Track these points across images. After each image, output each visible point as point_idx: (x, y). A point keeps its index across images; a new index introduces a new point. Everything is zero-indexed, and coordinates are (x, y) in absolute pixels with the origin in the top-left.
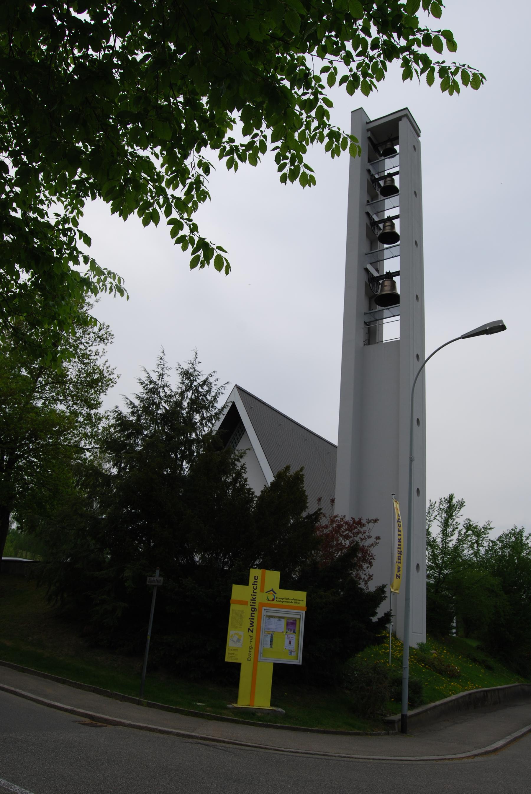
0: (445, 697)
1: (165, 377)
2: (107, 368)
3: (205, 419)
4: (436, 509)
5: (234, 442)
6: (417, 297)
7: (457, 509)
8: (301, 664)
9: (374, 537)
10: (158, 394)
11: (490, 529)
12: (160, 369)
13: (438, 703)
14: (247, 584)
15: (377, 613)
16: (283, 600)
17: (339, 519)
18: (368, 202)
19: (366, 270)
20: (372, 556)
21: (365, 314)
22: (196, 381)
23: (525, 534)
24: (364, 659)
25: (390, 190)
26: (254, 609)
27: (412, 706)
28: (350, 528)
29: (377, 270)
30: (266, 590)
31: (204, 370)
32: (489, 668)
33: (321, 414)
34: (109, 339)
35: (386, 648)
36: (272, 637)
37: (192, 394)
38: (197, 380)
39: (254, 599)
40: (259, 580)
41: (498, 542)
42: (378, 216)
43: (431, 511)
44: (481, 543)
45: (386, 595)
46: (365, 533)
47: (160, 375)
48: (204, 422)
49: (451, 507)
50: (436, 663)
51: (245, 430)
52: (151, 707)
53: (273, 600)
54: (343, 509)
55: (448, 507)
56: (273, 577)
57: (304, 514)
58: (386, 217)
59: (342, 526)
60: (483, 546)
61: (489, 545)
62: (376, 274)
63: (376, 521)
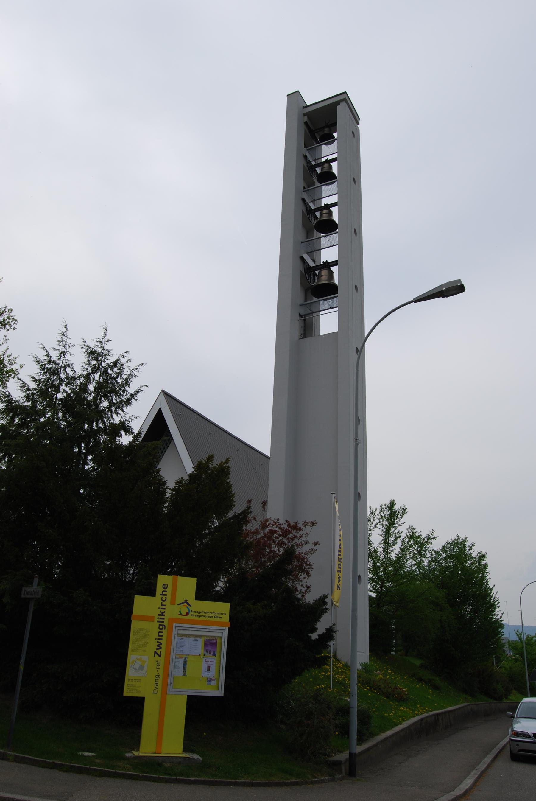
0: (396, 725)
1: (68, 356)
2: (9, 356)
3: (114, 404)
4: (377, 517)
5: (160, 452)
6: (356, 287)
7: (399, 516)
8: (222, 695)
9: (311, 542)
10: (58, 375)
11: (434, 538)
12: (61, 347)
13: (389, 733)
14: (154, 595)
15: (317, 629)
16: (201, 614)
17: (271, 522)
18: (304, 188)
19: (302, 258)
20: (309, 565)
21: (300, 305)
22: (105, 361)
23: (468, 544)
24: (303, 686)
25: (328, 177)
26: (162, 627)
27: (361, 740)
28: (285, 533)
29: (314, 261)
30: (178, 602)
31: (115, 350)
32: (435, 687)
33: (252, 422)
34: (12, 324)
35: (326, 671)
36: (185, 663)
37: (100, 376)
38: (106, 360)
39: (162, 614)
40: (169, 590)
41: (442, 553)
42: (314, 204)
43: (372, 519)
44: (424, 554)
45: (327, 607)
46: (301, 537)
47: (61, 354)
48: (113, 408)
49: (392, 514)
50: (383, 686)
51: (172, 439)
52: (19, 762)
53: (187, 614)
54: (277, 511)
55: (390, 515)
56: (188, 585)
57: (230, 515)
58: (323, 205)
59: (275, 532)
60: (427, 558)
61: (432, 556)
62: (312, 264)
63: (313, 524)
